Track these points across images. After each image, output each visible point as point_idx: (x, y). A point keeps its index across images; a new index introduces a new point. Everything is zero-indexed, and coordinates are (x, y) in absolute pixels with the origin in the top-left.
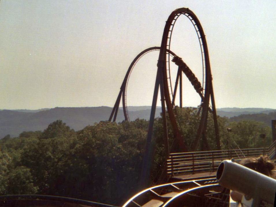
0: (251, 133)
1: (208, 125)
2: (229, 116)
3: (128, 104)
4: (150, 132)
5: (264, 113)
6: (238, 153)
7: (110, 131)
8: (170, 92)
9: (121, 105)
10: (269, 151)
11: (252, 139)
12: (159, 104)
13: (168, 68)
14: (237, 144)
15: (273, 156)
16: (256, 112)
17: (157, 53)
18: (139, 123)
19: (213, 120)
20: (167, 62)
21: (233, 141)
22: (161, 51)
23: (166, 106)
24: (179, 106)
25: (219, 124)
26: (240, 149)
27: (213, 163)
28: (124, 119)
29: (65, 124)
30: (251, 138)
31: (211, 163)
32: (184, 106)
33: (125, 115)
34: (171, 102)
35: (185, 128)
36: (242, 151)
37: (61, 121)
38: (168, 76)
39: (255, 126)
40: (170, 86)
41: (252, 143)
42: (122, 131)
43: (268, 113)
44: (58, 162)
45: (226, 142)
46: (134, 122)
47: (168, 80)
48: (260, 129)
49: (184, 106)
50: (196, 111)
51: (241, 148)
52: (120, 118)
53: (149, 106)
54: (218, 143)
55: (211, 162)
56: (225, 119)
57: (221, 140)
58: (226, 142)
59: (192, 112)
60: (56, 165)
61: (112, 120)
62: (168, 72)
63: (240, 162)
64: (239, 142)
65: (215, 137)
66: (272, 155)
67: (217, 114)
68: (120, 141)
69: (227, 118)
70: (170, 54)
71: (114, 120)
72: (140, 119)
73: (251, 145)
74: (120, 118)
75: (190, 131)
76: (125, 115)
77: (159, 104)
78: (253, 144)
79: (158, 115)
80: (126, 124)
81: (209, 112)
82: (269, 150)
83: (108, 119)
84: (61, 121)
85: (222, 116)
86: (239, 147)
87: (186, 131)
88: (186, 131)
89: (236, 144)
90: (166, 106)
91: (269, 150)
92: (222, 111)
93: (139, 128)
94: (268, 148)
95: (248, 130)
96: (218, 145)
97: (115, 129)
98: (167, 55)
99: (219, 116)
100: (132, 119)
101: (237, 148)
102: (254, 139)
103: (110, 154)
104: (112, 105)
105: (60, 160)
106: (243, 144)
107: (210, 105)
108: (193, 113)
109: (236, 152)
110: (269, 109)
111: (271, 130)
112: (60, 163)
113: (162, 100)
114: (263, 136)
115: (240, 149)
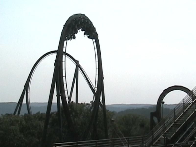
2: (117, 111)
3: (31, 101)
4: (46, 123)
5: (145, 108)
8: (66, 96)
9: (24, 101)
12: (55, 100)
13: (64, 68)
16: (135, 107)
17: (54, 56)
18: (39, 116)
20: (64, 62)
22: (57, 54)
23: (61, 102)
24: (75, 101)
26: (124, 138)
28: (27, 112)
32: (79, 102)
34: (68, 103)
36: (126, 139)
38: (64, 75)
40: (66, 90)
42: (24, 122)
43: (148, 108)
47: (64, 78)
49: (79, 102)
50: (89, 106)
51: (125, 137)
52: (24, 111)
53: (47, 103)
56: (113, 113)
57: (109, 130)
59: (85, 107)
62: (64, 70)
66: (149, 142)
67: (107, 108)
68: (22, 131)
69: (116, 112)
70: (66, 56)
74: (24, 111)
77: (55, 100)
79: (54, 109)
80: (28, 117)
81: (100, 106)
85: (111, 110)
86: (123, 136)
90: (61, 102)
92: (111, 106)
93: (39, 120)
94: (146, 136)
97: (17, 121)
98: (64, 56)
100: (34, 112)
104: (17, 101)
107: (101, 100)
108: (87, 108)
110: (147, 105)
113: (58, 96)
114: (142, 126)
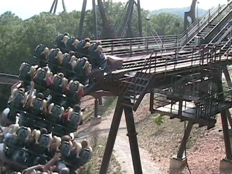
0: (168, 22)
1: (133, 16)
6: (156, 38)
7: (50, 21)
10: (180, 38)
11: (168, 28)
14: (156, 31)
15: (183, 43)
19: (138, 12)
21: (152, 29)
25: (143, 15)
27: (131, 49)
28: (63, 10)
29: (14, 14)
30: (167, 26)
31: (129, 49)
33: (64, 7)
35: (112, 19)
37: (11, 11)
39: (172, 17)
41: (167, 31)
44: (6, 45)
45: (148, 30)
46: (71, 13)
48: (175, 20)
54: (140, 30)
55: (129, 48)
58: (148, 30)
60: (5, 48)
61: (53, 12)
63: (198, 10)
64: (157, 30)
65: (138, 26)
69: (150, 11)
71: (55, 11)
72: (76, 11)
73: (166, 33)
75: (119, 21)
76: (64, 7)
78: (168, 32)
80: (64, 14)
82: (181, 37)
83: (49, 11)
84: (11, 11)
87: (115, 21)
88: (115, 21)
89: (155, 31)
91: (181, 37)
95: (165, 21)
96: (140, 32)
99: (142, 9)
101: (101, 60)
102: (169, 27)
103: (49, 40)
105: (7, 43)
106: (160, 32)
109: (155, 39)
111: (184, 20)
112: (8, 46)
115: (153, 37)
